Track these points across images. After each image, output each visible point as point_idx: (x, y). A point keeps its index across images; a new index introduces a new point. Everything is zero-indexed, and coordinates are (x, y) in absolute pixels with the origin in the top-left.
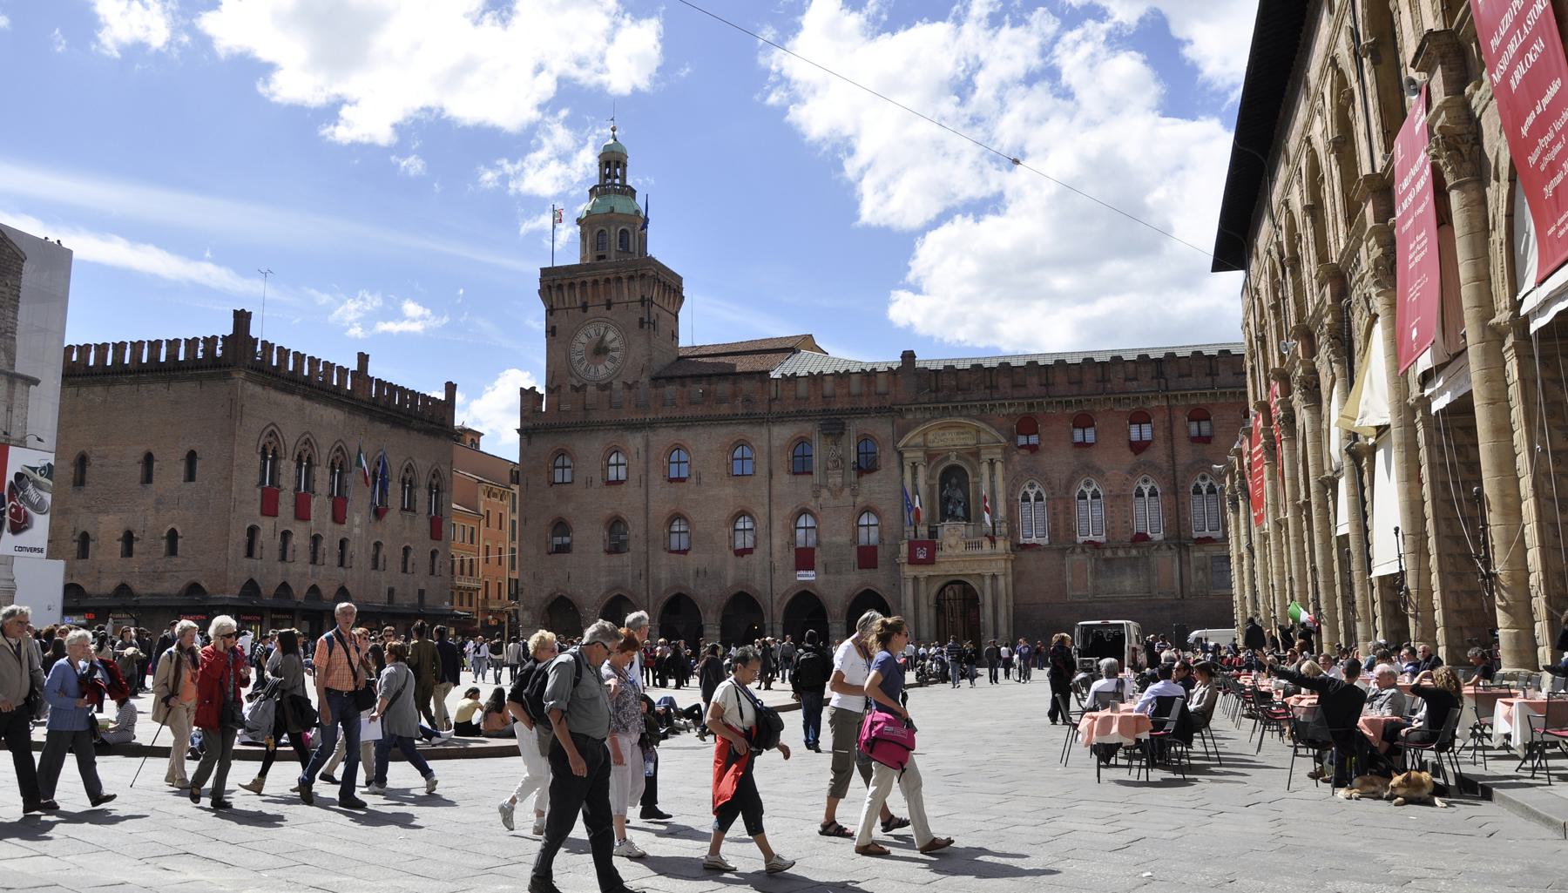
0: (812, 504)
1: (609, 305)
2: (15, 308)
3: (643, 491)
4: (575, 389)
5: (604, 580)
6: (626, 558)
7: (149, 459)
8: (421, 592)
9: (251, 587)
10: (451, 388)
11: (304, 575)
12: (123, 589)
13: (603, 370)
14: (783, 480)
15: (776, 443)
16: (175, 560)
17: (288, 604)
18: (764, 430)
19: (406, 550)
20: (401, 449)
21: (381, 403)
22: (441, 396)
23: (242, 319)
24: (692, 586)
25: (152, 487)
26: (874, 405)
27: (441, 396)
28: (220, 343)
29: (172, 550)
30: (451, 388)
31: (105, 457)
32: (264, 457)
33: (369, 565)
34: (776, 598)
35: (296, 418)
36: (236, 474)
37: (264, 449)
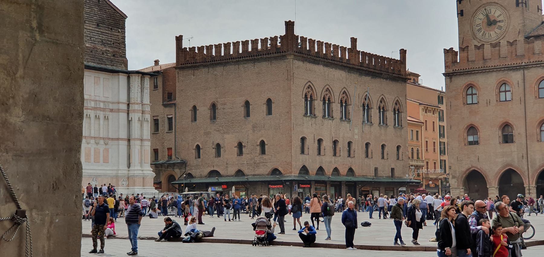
3: (523, 106)
4: (477, 48)
8: (393, 170)
9: (304, 170)
10: (403, 52)
11: (331, 162)
12: (239, 173)
16: (264, 156)
17: (323, 178)
19: (367, 145)
20: (378, 89)
22: (398, 58)
23: (290, 25)
25: (250, 119)
27: (398, 58)
28: (279, 40)
30: (403, 52)
32: (306, 100)
35: (323, 77)
36: (293, 110)
37: (306, 95)
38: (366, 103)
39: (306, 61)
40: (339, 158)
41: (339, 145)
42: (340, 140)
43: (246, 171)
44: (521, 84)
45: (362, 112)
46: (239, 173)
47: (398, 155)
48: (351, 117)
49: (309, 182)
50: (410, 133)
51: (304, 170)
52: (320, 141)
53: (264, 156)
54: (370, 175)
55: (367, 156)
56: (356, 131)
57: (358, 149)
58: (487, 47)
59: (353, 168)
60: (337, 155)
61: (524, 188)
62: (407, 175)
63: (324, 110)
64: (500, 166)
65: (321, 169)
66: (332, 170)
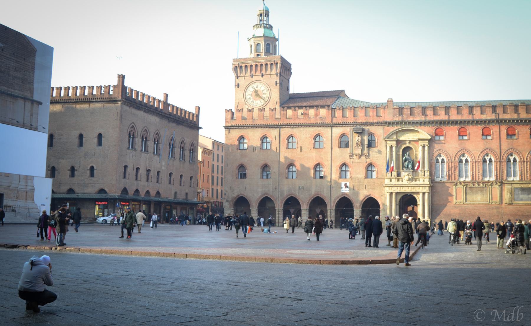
0: (348, 161)
1: (262, 76)
2: (33, 72)
5: (260, 190)
6: (270, 182)
7: (81, 136)
8: (187, 194)
9: (125, 191)
12: (71, 191)
13: (259, 103)
14: (337, 150)
15: (334, 135)
17: (138, 198)
18: (329, 130)
19: (171, 174)
20: (168, 131)
21: (173, 115)
22: (193, 111)
23: (122, 78)
24: (325, 195)
26: (375, 121)
28: (112, 88)
29: (92, 175)
31: (62, 135)
33: (168, 182)
34: (333, 199)
37: (130, 133)
38: (172, 143)
39: (132, 106)
40: (151, 183)
41: (151, 174)
42: (152, 169)
43: (76, 189)
44: (278, 138)
45: (168, 149)
46: (71, 191)
47: (191, 183)
48: (161, 152)
49: (139, 201)
50: (420, 148)
51: (125, 191)
52: (138, 169)
53: (92, 178)
54: (172, 198)
55: (170, 183)
56: (163, 163)
57: (164, 176)
58: (256, 112)
59: (160, 192)
60: (149, 180)
61: (275, 210)
62: (196, 199)
63: (142, 145)
64: (259, 195)
65: (137, 191)
66: (145, 192)
